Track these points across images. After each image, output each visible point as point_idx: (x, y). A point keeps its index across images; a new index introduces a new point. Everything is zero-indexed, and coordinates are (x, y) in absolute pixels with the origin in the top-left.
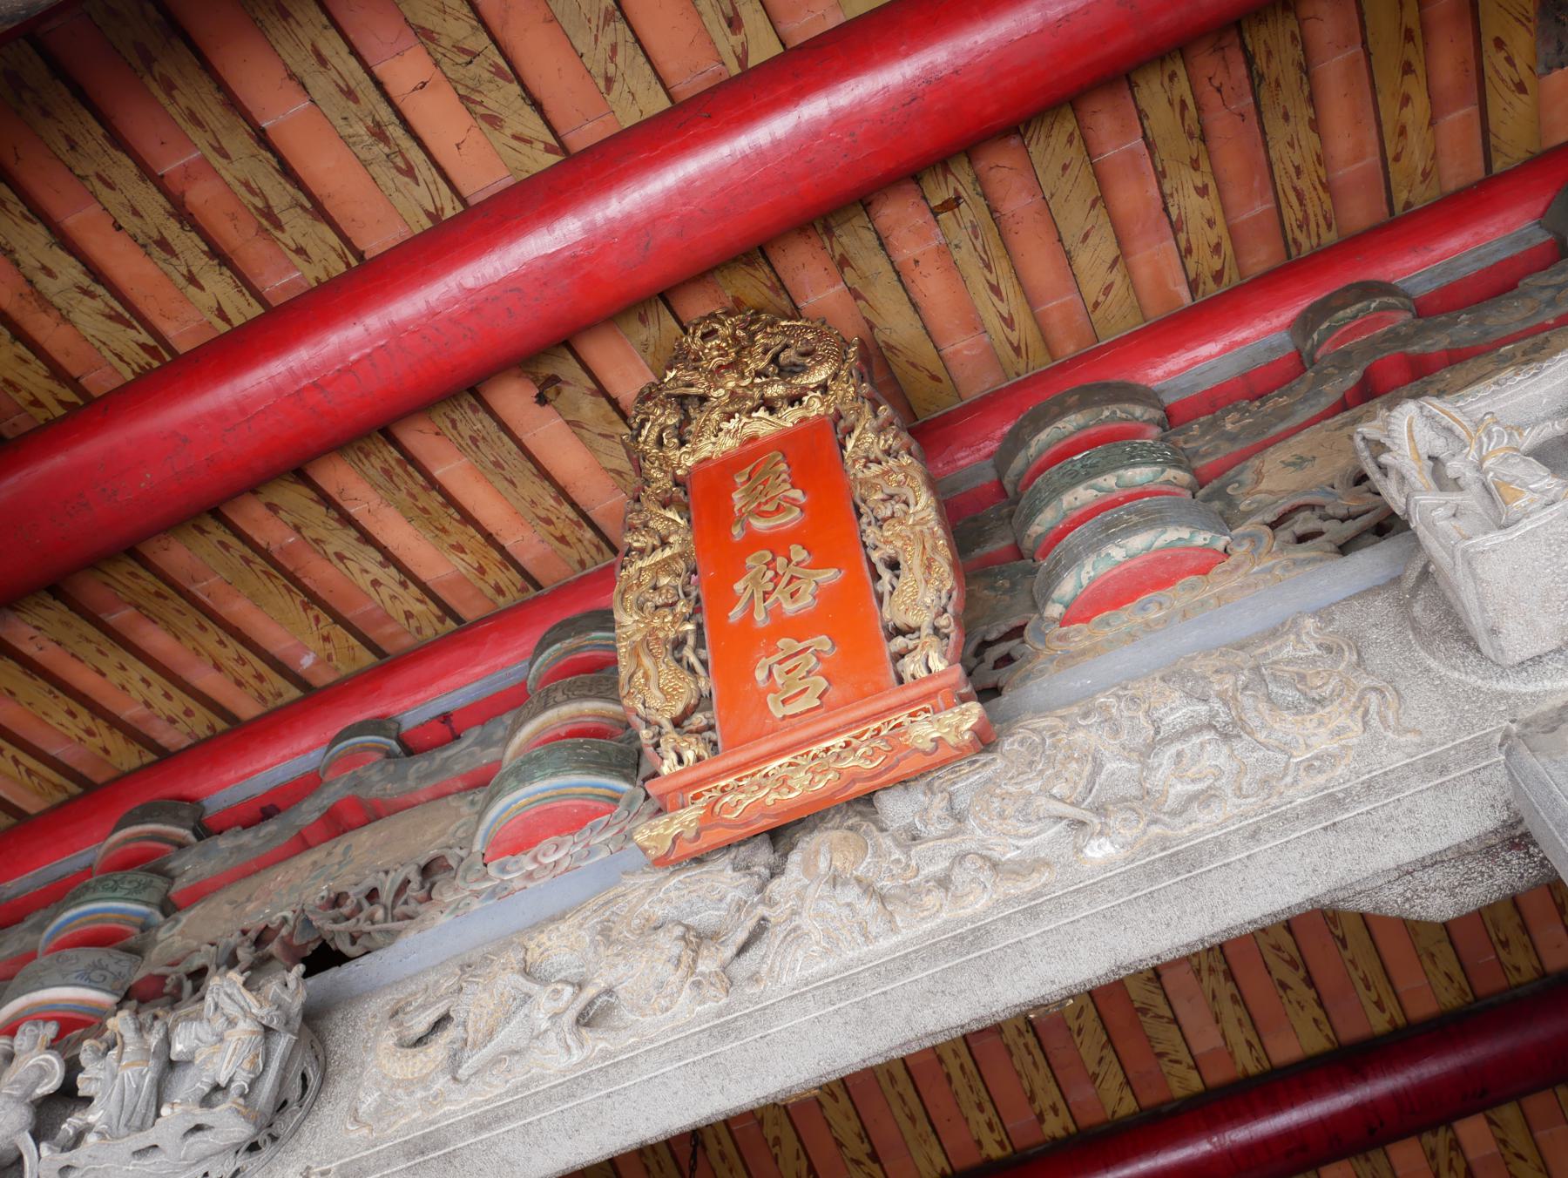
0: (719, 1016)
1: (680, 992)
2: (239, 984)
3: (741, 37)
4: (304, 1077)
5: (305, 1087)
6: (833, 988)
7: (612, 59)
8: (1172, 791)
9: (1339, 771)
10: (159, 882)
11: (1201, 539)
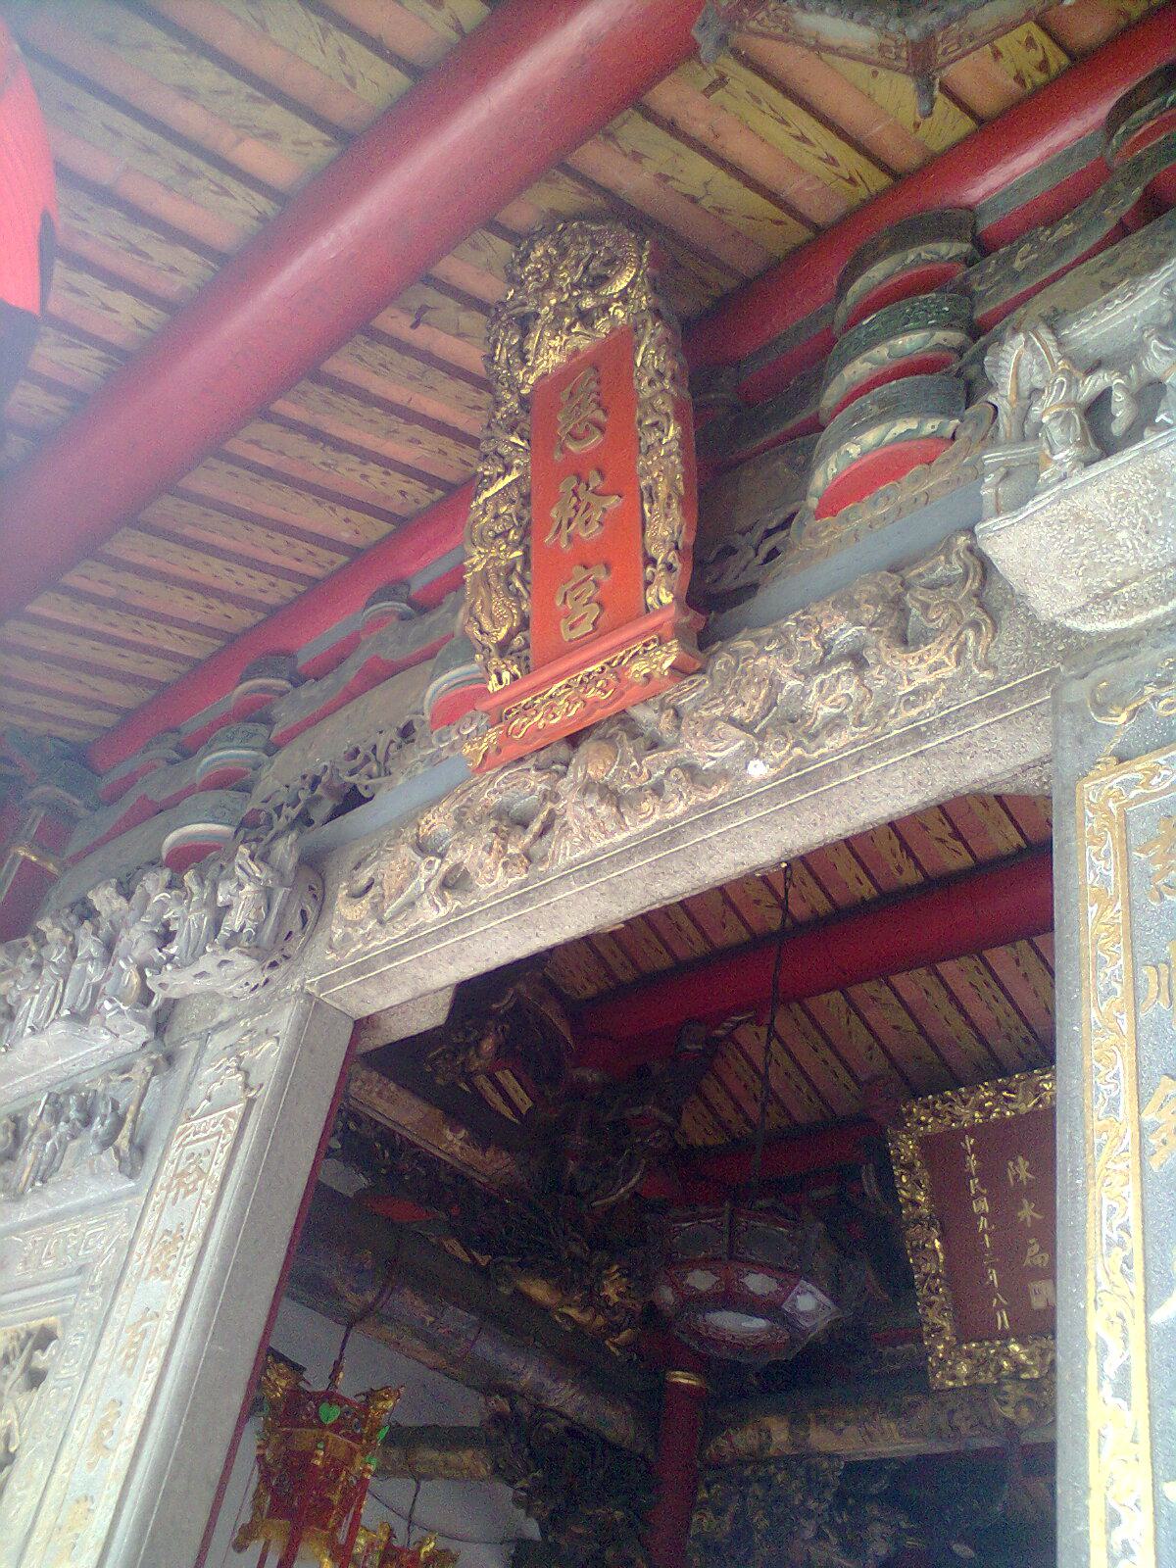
0: (521, 888)
1: (496, 869)
2: (247, 855)
3: (446, 10)
4: (303, 913)
5: (305, 922)
6: (584, 872)
7: (344, 61)
8: (821, 713)
9: (929, 705)
10: (262, 729)
11: (930, 426)
